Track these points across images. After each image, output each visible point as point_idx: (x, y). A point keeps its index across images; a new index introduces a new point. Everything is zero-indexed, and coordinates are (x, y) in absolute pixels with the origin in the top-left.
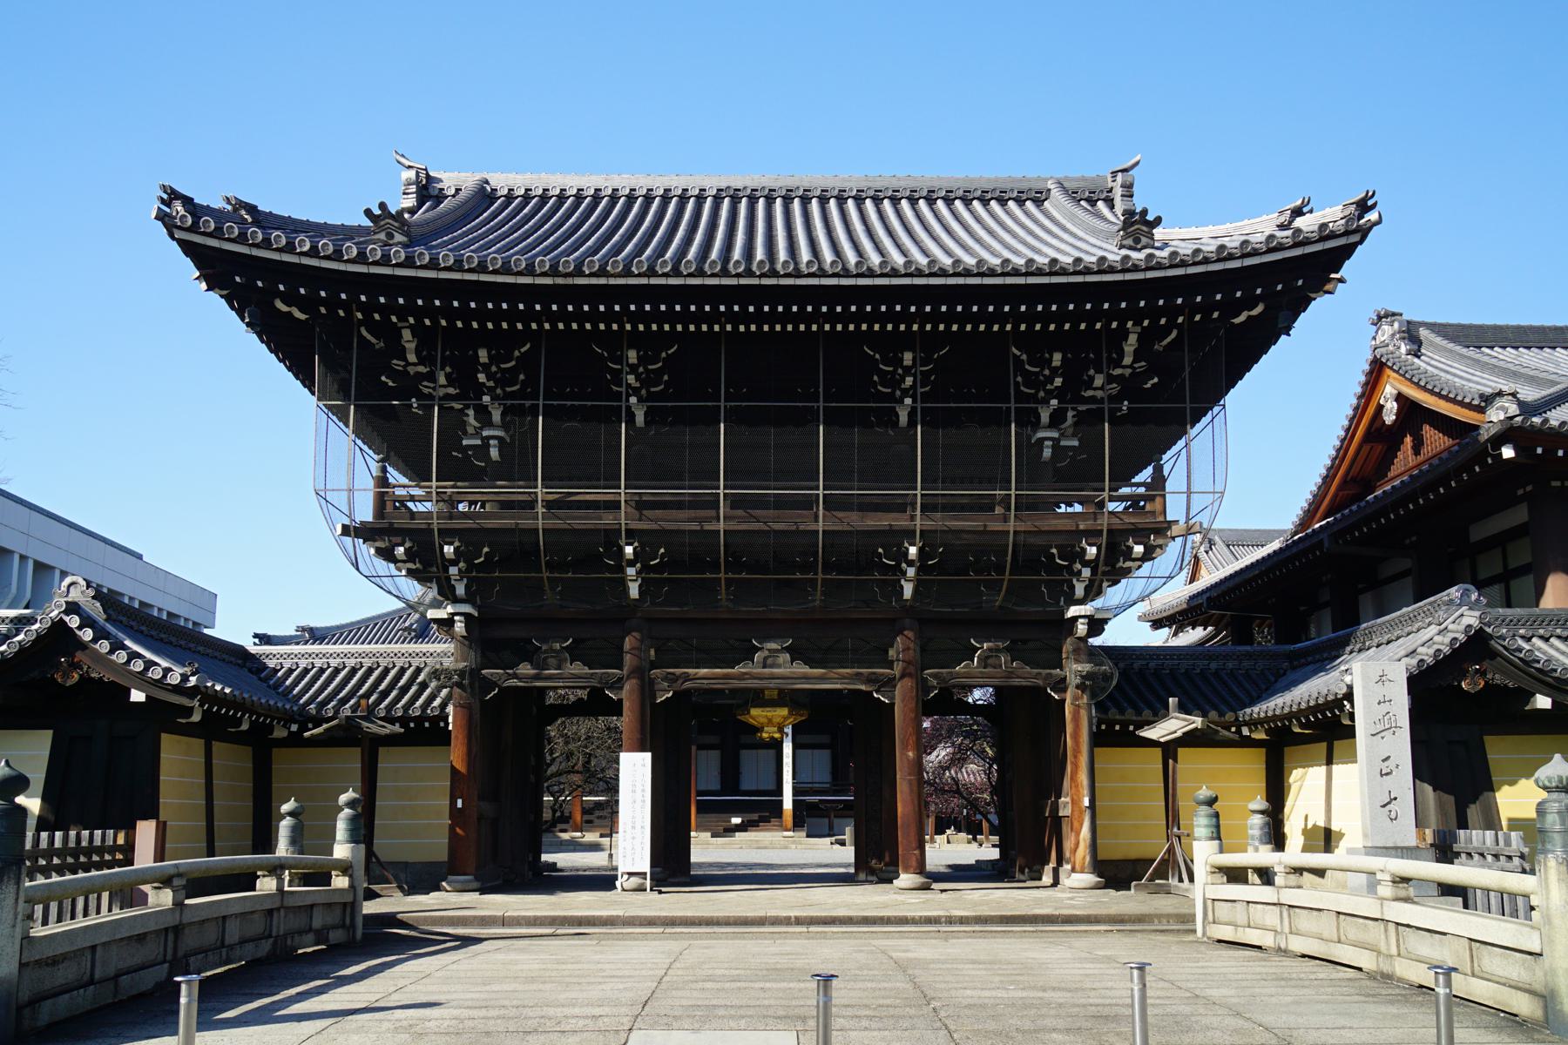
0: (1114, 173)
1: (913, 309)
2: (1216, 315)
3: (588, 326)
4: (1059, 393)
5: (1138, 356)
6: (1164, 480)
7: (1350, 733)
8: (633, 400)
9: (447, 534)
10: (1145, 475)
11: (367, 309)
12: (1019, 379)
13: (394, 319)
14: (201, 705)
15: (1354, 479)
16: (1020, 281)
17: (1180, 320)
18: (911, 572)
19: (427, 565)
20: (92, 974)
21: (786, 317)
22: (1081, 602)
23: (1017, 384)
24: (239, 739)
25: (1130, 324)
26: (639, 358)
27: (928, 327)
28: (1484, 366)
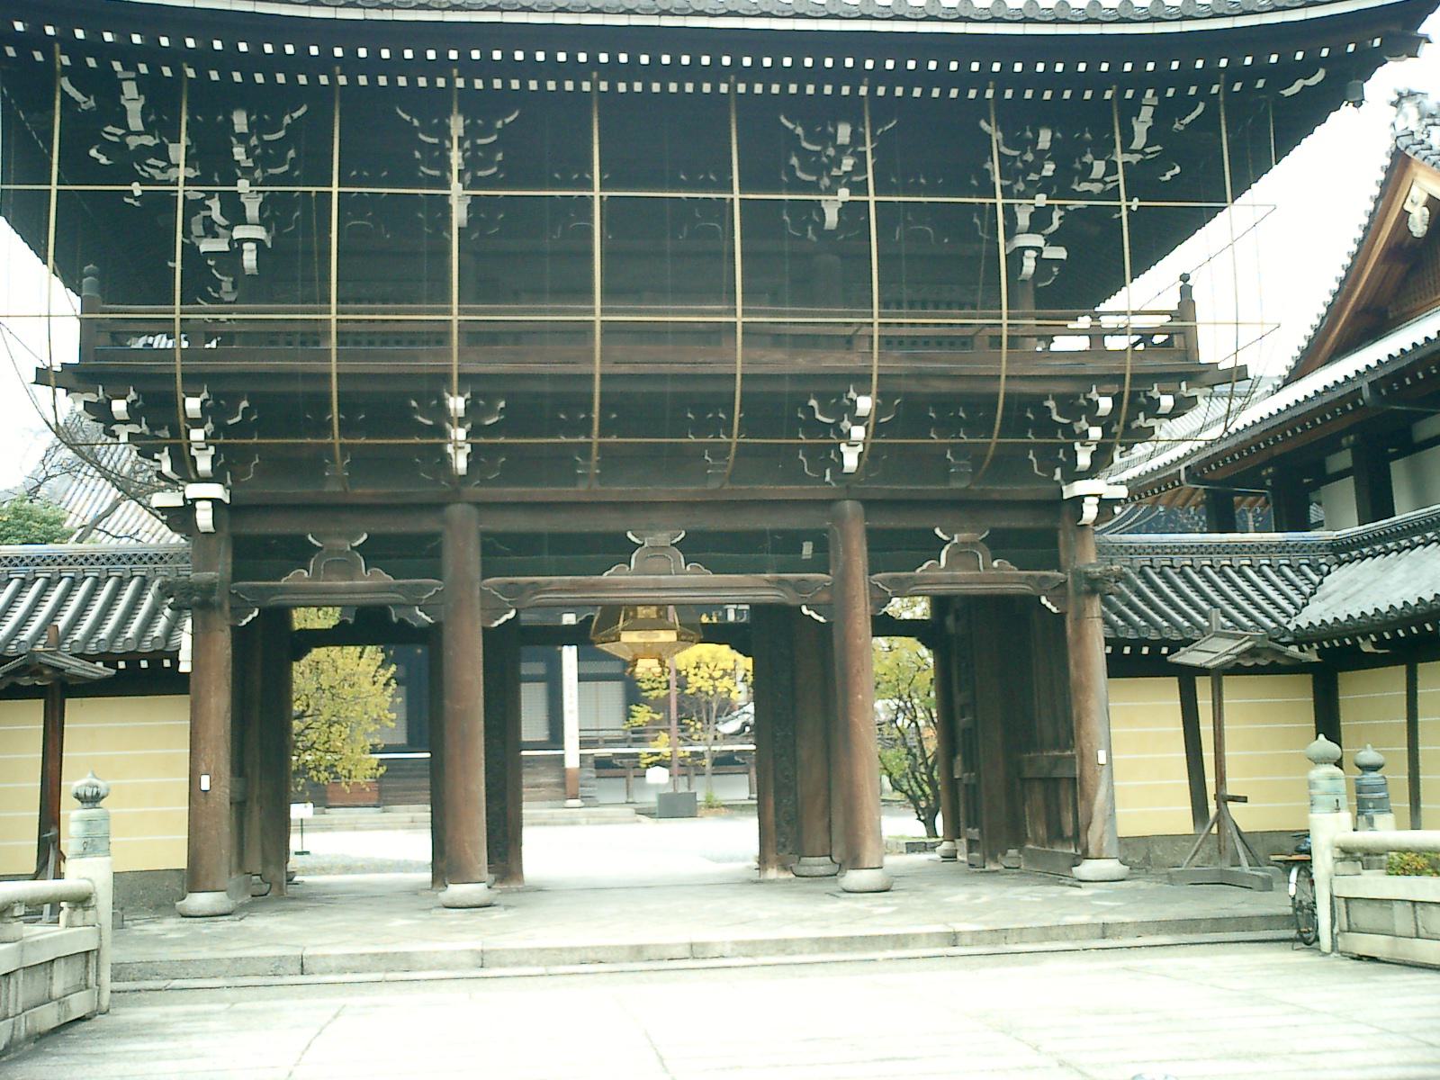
2: (1260, 84)
3: (363, 80)
9: (194, 382)
17: (1215, 89)
22: (1091, 473)
26: (250, 125)
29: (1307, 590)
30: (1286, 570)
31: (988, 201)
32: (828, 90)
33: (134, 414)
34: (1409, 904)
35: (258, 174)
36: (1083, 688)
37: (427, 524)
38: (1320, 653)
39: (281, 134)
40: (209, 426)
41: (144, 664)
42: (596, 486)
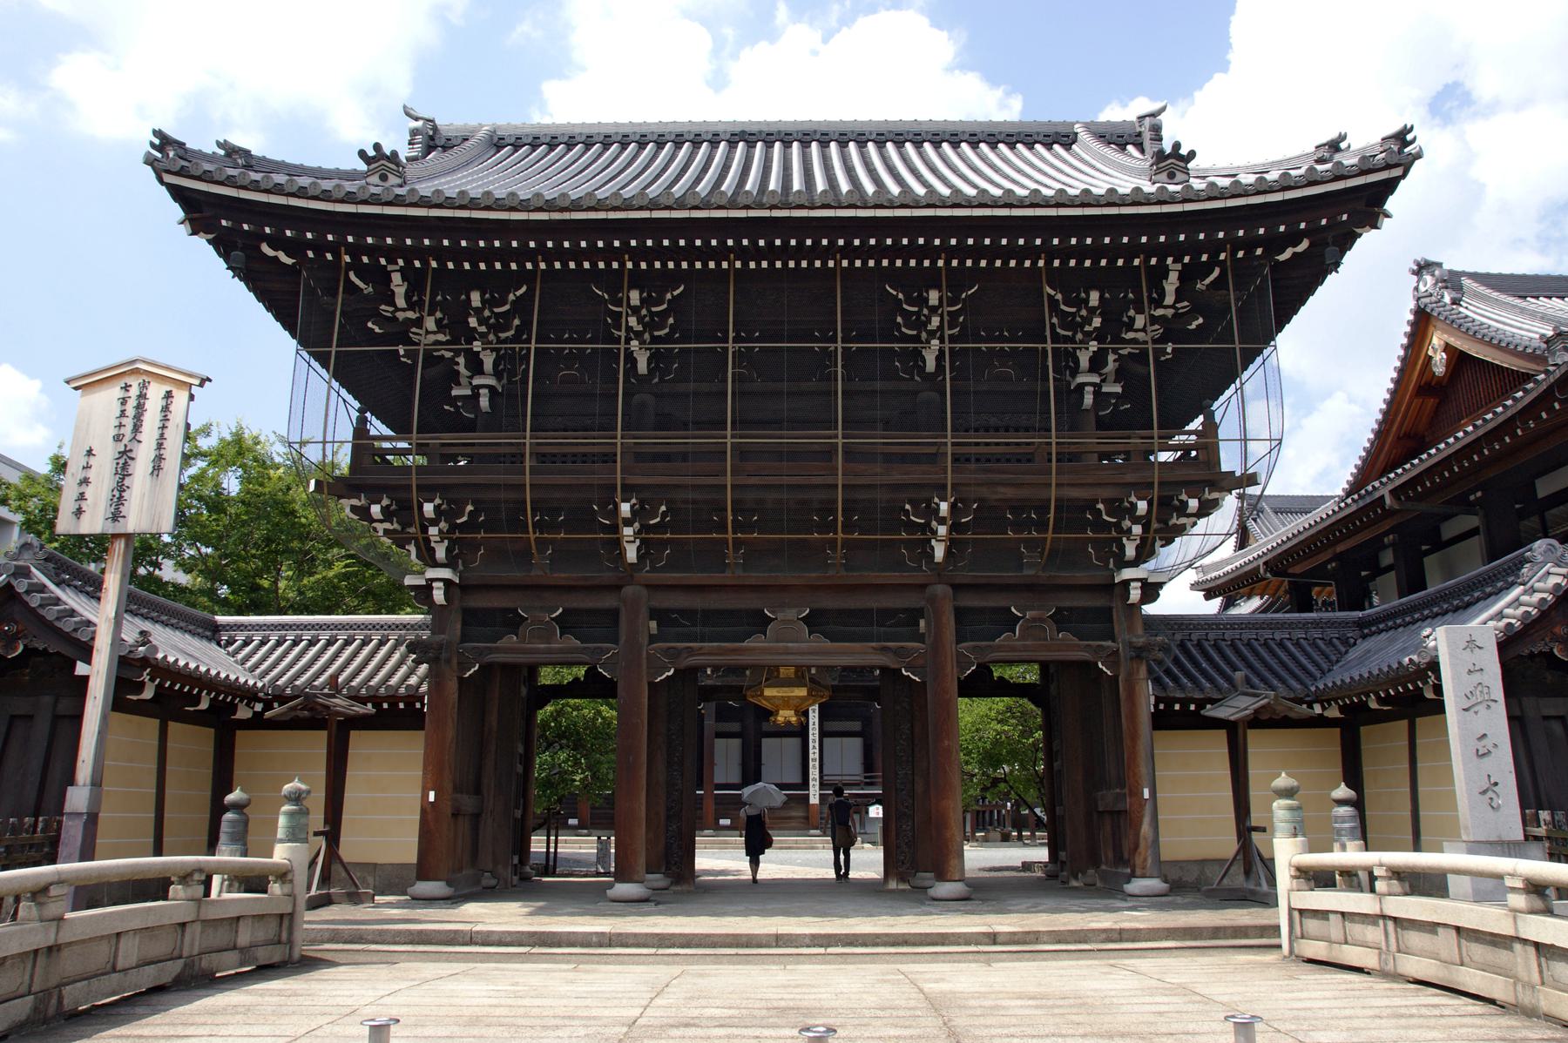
0: (1141, 118)
2: (1259, 251)
4: (1099, 336)
5: (1180, 294)
6: (1216, 427)
7: (1438, 707)
8: (635, 343)
9: (428, 491)
10: (1197, 423)
11: (355, 251)
12: (1055, 320)
13: (383, 261)
14: (152, 680)
15: (1407, 436)
17: (1222, 256)
18: (942, 530)
20: (30, 986)
22: (1135, 563)
23: (1053, 326)
24: (199, 719)
25: (1170, 260)
26: (642, 300)
27: (955, 263)
28: (1533, 315)
29: (1334, 658)
31: (1040, 346)
33: (387, 514)
34: (1453, 933)
36: (1134, 737)
37: (607, 602)
38: (1341, 709)
39: (507, 307)
40: (637, 525)
41: (401, 706)
42: (740, 572)
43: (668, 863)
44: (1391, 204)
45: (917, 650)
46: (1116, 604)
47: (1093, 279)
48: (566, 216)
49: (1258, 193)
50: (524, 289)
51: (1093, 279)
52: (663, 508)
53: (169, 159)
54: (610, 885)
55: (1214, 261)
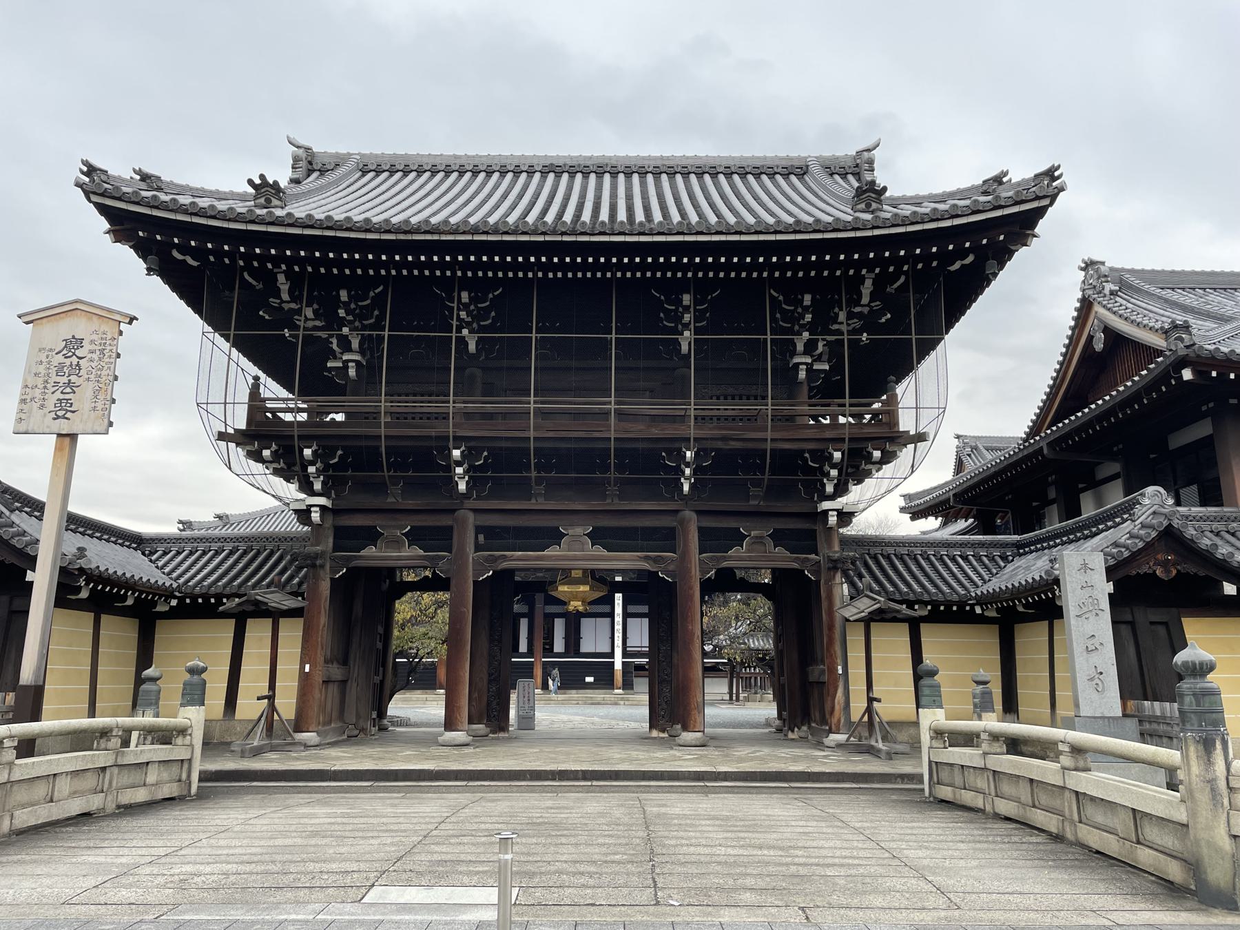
1: (685, 260)
2: (935, 264)
8: (465, 332)
9: (307, 439)
11: (249, 257)
13: (269, 266)
14: (87, 584)
16: (772, 238)
17: (906, 268)
18: (688, 471)
19: (290, 465)
21: (585, 266)
22: (832, 497)
25: (864, 271)
29: (994, 571)
30: (985, 559)
32: (649, 274)
35: (475, 325)
37: (444, 521)
38: (998, 610)
39: (368, 302)
43: (488, 716)
44: (1042, 227)
45: (444, 557)
46: (819, 528)
47: (807, 285)
48: (409, 237)
49: (932, 220)
50: (381, 288)
51: (807, 285)
52: (486, 453)
53: (95, 185)
54: (441, 735)
55: (898, 273)
